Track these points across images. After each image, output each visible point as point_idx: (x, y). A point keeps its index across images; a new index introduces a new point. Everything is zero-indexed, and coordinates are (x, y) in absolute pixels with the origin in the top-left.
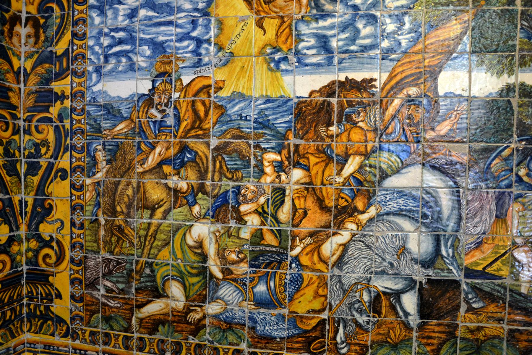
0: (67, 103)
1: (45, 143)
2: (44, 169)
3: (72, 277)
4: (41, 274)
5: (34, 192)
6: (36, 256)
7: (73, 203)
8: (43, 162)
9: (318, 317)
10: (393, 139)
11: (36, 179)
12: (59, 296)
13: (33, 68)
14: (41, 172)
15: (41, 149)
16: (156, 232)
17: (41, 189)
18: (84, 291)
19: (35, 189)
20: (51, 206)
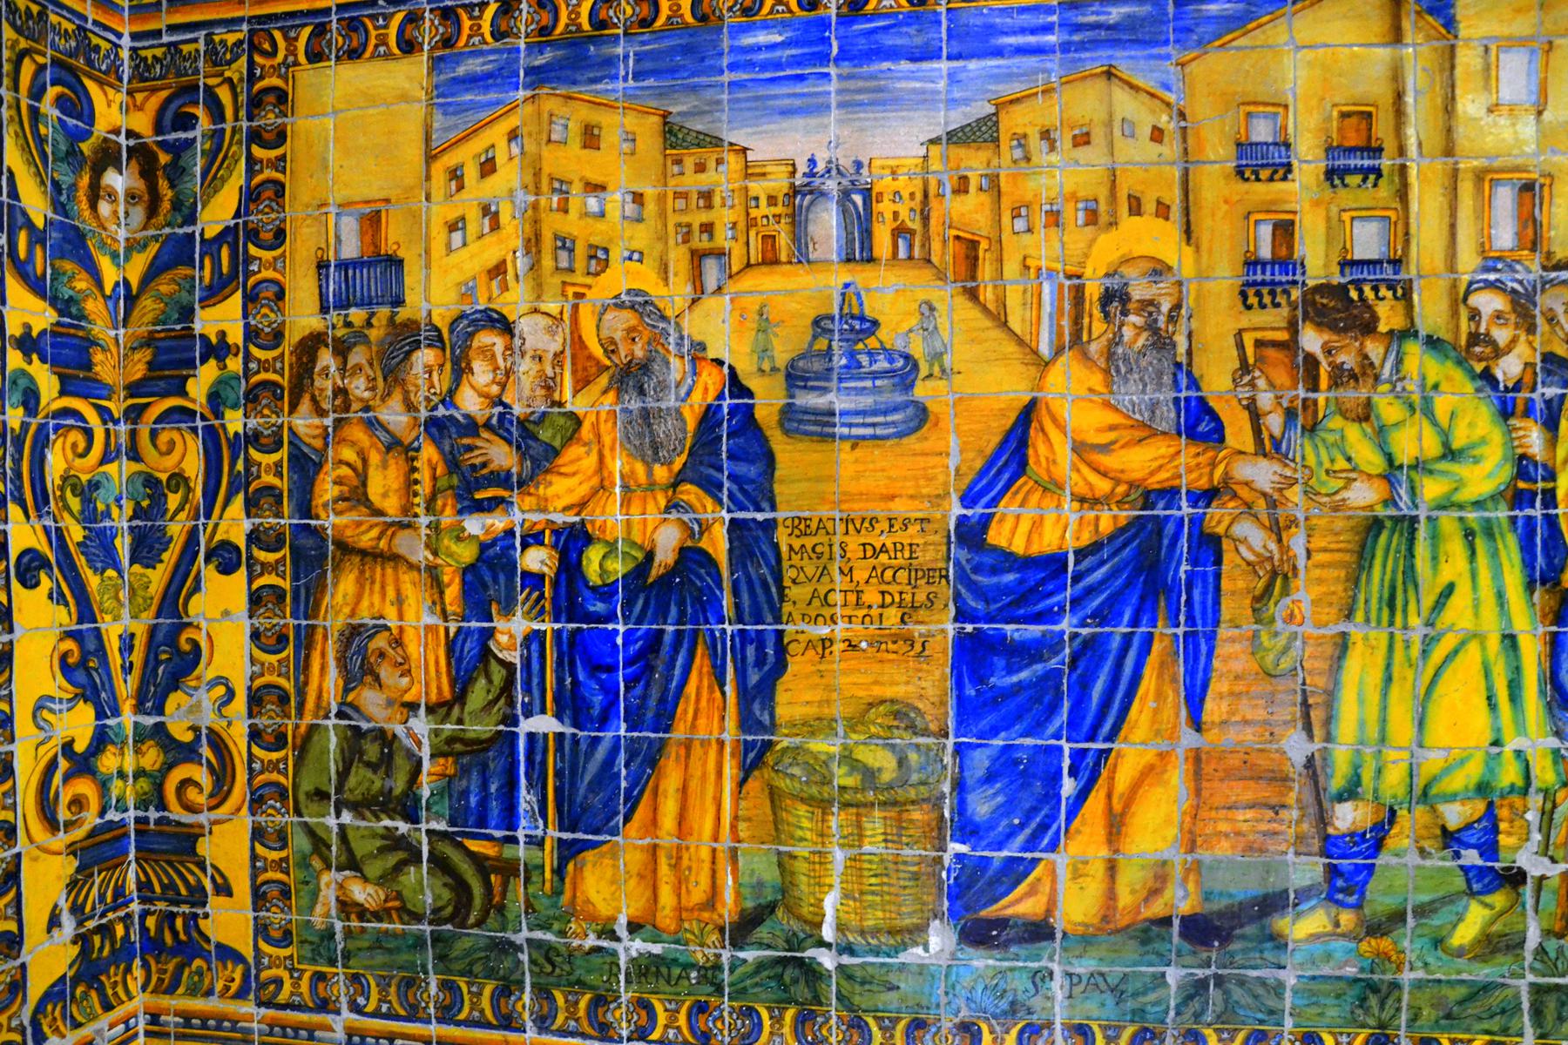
0: (235, 364)
1: (178, 480)
3: (258, 682)
4: (175, 835)
5: (154, 608)
6: (159, 788)
8: (177, 529)
11: (157, 577)
12: (224, 889)
13: (149, 278)
14: (170, 556)
15: (165, 496)
17: (173, 602)
18: (294, 917)
19: (156, 601)
20: (196, 646)
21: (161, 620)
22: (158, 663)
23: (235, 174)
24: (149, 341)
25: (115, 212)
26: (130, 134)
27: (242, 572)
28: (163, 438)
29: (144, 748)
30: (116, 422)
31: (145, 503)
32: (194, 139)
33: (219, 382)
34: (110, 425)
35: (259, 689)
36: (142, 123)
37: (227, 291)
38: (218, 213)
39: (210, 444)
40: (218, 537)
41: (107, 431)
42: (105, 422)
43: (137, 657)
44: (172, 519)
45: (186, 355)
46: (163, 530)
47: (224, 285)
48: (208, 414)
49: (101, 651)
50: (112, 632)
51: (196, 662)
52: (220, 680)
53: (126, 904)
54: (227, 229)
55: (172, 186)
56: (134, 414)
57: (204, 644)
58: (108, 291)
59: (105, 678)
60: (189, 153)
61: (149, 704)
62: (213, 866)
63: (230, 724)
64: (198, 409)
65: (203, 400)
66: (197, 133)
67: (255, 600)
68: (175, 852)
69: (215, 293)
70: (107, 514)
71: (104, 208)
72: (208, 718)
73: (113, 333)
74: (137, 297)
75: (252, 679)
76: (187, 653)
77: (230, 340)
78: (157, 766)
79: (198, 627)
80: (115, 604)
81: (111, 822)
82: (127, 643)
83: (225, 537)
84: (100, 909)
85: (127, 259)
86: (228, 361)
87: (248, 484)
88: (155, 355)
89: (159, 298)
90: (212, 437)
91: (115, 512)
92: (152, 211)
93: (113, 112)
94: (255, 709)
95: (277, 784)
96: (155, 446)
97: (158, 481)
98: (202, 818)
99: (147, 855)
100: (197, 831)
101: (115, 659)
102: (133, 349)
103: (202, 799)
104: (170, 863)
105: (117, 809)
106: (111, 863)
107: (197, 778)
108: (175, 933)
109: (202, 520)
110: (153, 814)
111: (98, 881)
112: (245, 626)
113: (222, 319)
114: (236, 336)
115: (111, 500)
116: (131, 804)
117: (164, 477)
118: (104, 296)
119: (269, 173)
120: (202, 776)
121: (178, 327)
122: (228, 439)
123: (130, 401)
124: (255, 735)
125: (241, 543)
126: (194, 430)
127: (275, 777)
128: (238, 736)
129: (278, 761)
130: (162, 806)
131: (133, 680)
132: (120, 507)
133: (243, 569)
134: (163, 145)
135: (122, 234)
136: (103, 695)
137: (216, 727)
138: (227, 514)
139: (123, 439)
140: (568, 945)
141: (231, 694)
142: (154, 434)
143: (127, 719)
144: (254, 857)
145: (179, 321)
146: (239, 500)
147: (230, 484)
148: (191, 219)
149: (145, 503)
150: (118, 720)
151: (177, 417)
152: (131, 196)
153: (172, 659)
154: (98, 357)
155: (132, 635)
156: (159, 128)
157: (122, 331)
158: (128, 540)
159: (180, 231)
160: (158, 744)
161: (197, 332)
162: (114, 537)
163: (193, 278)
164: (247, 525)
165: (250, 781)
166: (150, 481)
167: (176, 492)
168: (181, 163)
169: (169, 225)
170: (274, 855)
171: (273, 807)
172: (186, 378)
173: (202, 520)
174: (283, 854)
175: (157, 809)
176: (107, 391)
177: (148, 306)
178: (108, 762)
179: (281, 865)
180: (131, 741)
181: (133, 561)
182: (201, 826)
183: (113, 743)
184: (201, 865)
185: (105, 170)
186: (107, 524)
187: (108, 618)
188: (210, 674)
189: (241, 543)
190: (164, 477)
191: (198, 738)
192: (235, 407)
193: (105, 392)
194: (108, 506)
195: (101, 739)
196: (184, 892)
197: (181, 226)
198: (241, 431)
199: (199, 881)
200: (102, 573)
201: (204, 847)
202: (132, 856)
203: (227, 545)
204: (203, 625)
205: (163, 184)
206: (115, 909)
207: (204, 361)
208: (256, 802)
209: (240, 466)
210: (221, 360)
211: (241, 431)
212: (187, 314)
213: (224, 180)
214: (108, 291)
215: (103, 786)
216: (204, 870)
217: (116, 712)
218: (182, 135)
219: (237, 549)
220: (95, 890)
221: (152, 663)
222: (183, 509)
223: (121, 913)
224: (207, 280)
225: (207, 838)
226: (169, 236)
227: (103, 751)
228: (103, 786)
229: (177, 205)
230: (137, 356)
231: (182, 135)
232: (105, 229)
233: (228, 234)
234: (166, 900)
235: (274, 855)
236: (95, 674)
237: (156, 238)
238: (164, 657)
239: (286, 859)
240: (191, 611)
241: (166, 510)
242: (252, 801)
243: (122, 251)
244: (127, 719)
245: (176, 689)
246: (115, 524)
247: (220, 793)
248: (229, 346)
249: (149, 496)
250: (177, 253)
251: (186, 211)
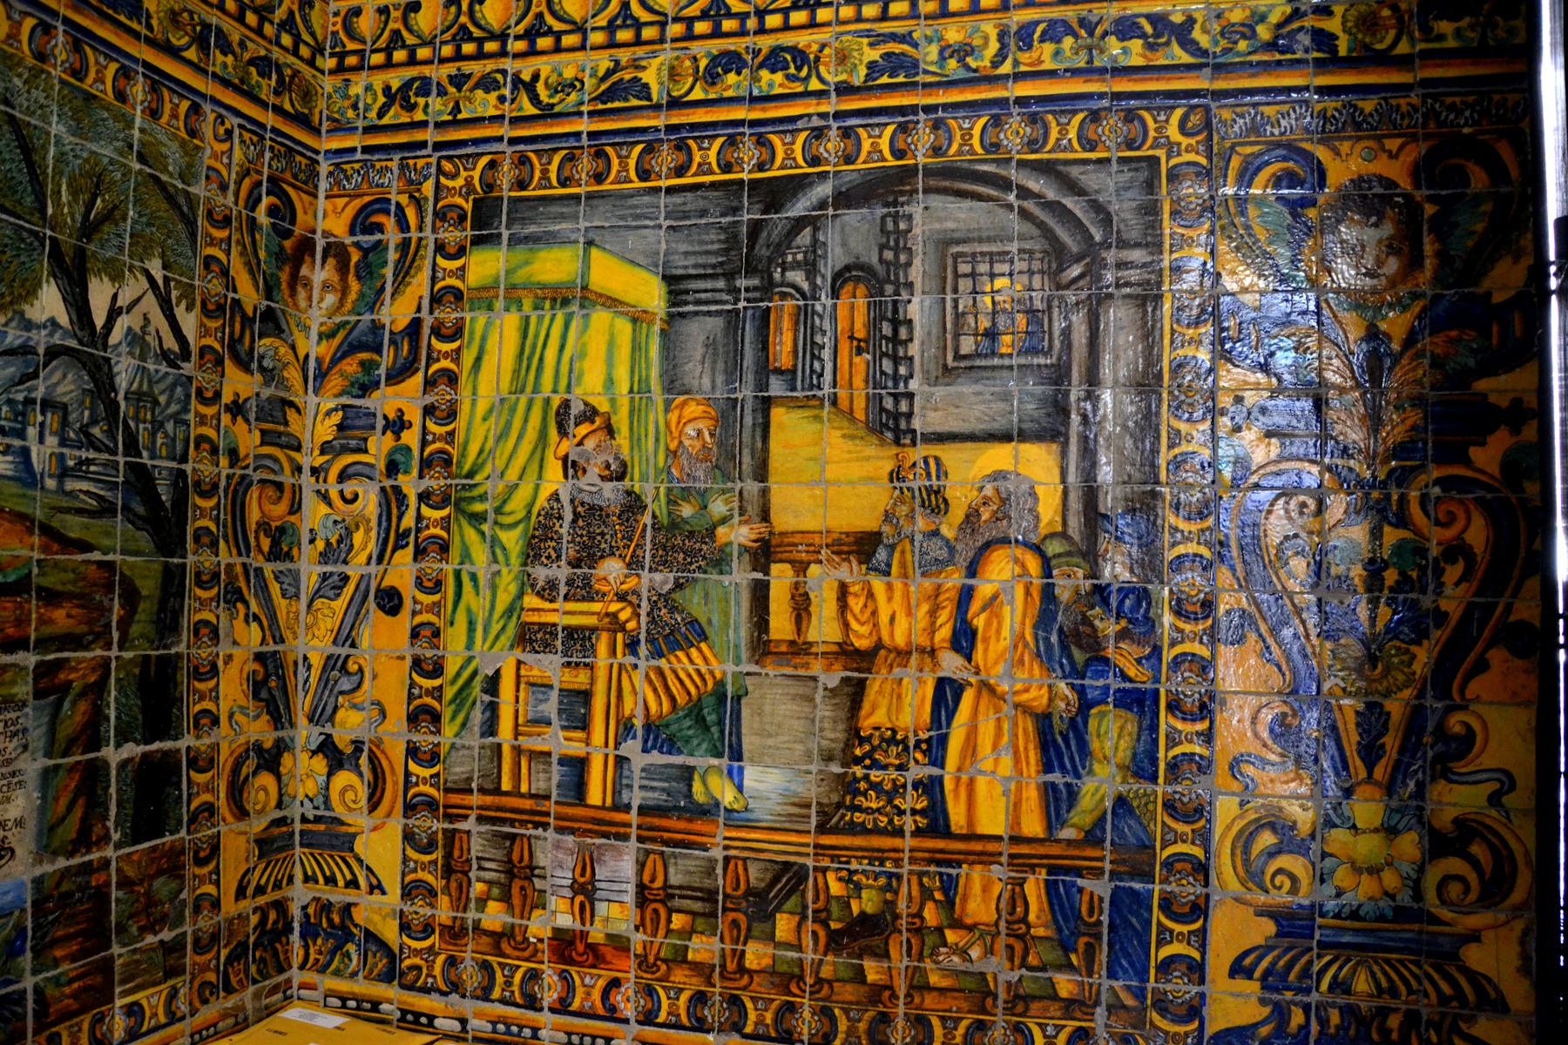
13: (335, 361)
38: (396, 313)
69: (398, 375)
108: (330, 921)
114: (414, 415)
119: (445, 363)
122: (397, 530)
124: (412, 752)
128: (397, 752)
208: (410, 809)
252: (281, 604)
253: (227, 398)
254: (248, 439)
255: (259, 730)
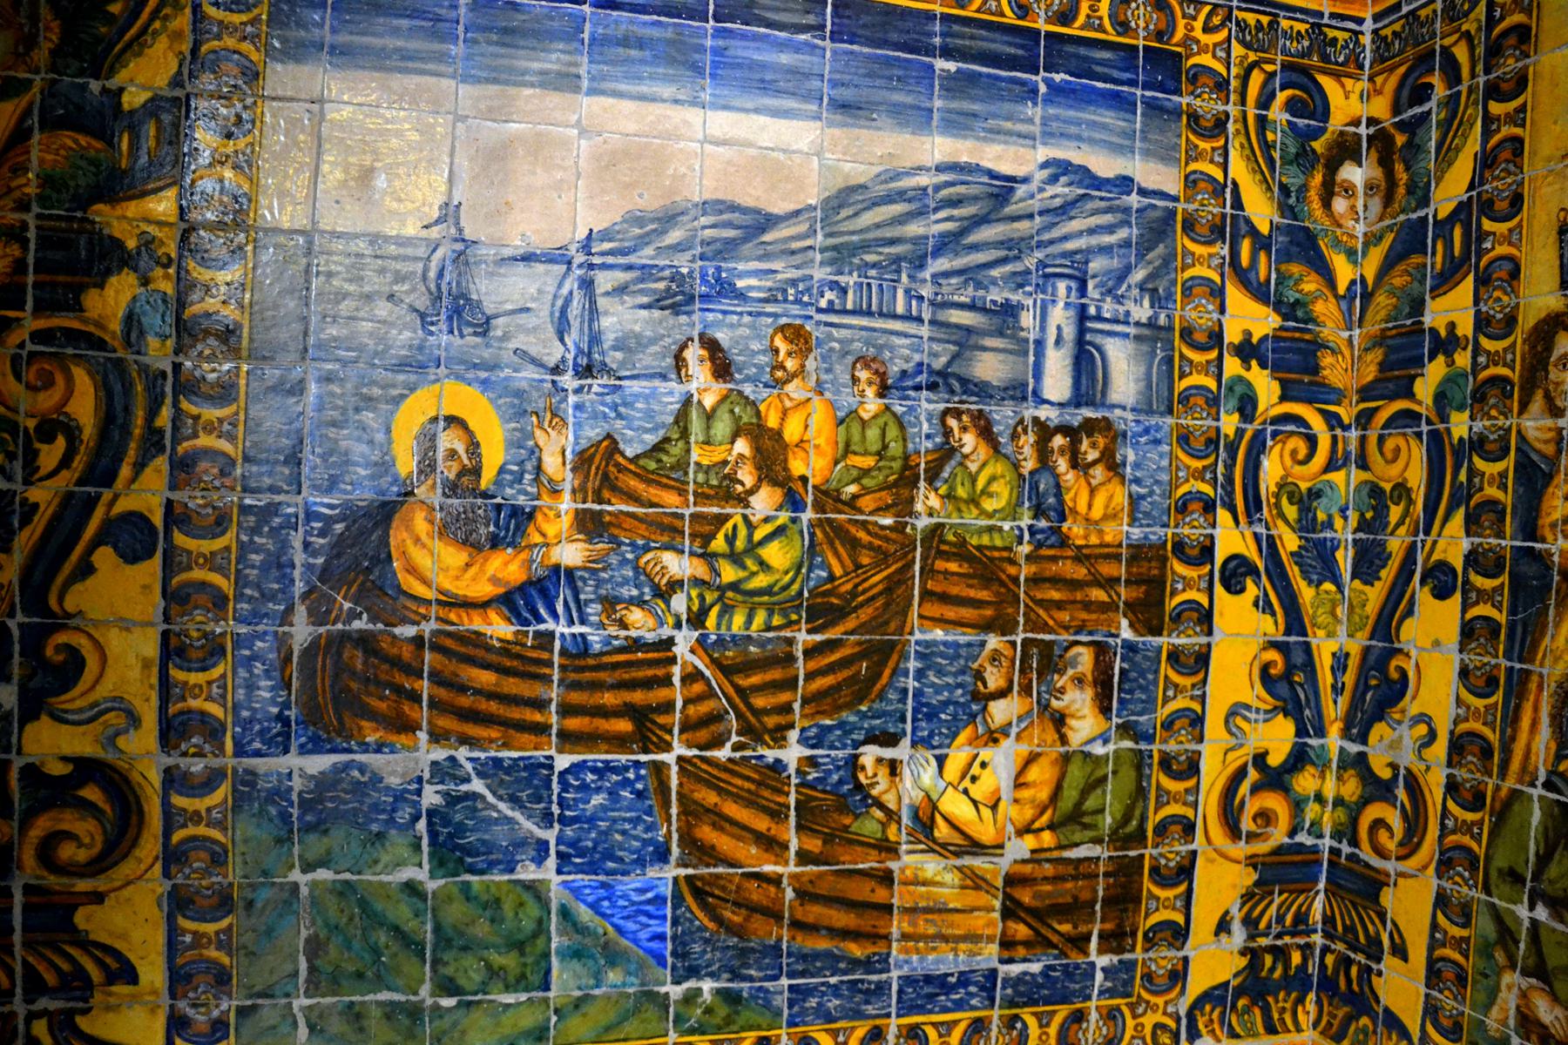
0: (1463, 359)
1: (1402, 491)
2: (1396, 565)
3: (1463, 727)
4: (1362, 877)
5: (1369, 628)
6: (1354, 822)
7: (1201, 675)
8: (1396, 545)
9: (790, 907)
10: (979, 548)
11: (1374, 595)
14: (1388, 574)
15: (1387, 507)
16: (398, 690)
17: (1386, 625)
19: (1371, 622)
20: (1404, 674)
21: (1373, 643)
22: (1367, 688)
23: (1470, 141)
24: (1380, 340)
25: (1353, 207)
26: (1372, 121)
27: (1458, 597)
28: (1390, 444)
29: (1346, 776)
30: (1346, 428)
31: (1369, 515)
32: (1429, 112)
33: (1448, 380)
34: (1338, 432)
35: (1461, 736)
36: (1380, 107)
37: (1458, 276)
38: (1451, 189)
39: (1434, 453)
40: (1435, 557)
41: (1334, 438)
42: (1332, 428)
43: (1349, 678)
44: (1392, 533)
45: (1415, 353)
46: (1383, 544)
47: (1461, 266)
48: (1434, 418)
49: (1309, 666)
50: (1325, 649)
51: (1403, 694)
52: (1423, 718)
53: (1308, 933)
54: (1460, 203)
55: (1407, 169)
56: (1364, 419)
57: (1411, 675)
58: (1341, 290)
59: (1312, 697)
60: (1424, 128)
61: (1355, 731)
62: (1394, 923)
63: (1428, 768)
64: (1424, 412)
65: (1429, 401)
66: (1432, 104)
67: (1468, 632)
68: (1358, 893)
69: (1445, 281)
70: (1329, 524)
71: (1340, 205)
72: (1407, 759)
73: (1346, 334)
74: (1372, 294)
75: (1455, 723)
76: (1395, 682)
77: (1459, 332)
78: (1354, 799)
79: (1408, 655)
80: (1330, 619)
81: (1301, 844)
82: (1340, 662)
83: (1441, 556)
84: (1276, 929)
85: (1364, 254)
86: (1456, 356)
87: (1470, 497)
88: (1386, 355)
89: (1392, 294)
90: (1436, 442)
91: (1338, 523)
92: (1388, 200)
93: (1350, 103)
94: (1456, 758)
95: (1469, 850)
96: (1382, 454)
97: (1382, 491)
98: (1390, 866)
99: (1334, 888)
100: (1382, 878)
101: (1326, 678)
102: (1366, 350)
103: (1391, 846)
104: (1354, 905)
105: (1309, 833)
106: (1292, 887)
107: (1389, 821)
109: (1421, 536)
110: (1346, 849)
111: (1277, 901)
112: (1455, 659)
113: (1453, 309)
115: (1334, 511)
116: (1327, 830)
117: (1387, 487)
118: (1336, 296)
120: (1395, 820)
121: (1409, 322)
122: (1452, 445)
123: (1363, 406)
124: (1452, 787)
125: (1458, 564)
126: (1419, 435)
127: (1467, 840)
128: (1434, 784)
129: (1473, 823)
130: (1354, 843)
131: (1343, 701)
132: (1345, 518)
133: (1458, 596)
134: (1400, 126)
135: (1360, 229)
136: (1307, 712)
137: (1415, 770)
138: (1446, 532)
139: (1353, 447)
140: (1106, 875)
141: (1432, 736)
142: (1381, 440)
143: (1334, 741)
144: (1434, 926)
145: (1409, 316)
146: (1459, 517)
147: (1452, 495)
148: (1425, 202)
149: (1369, 515)
150: (1321, 741)
151: (1400, 422)
152: (1370, 187)
153: (1381, 688)
154: (1327, 360)
155: (1347, 655)
156: (1396, 109)
157: (1357, 331)
158: (1351, 553)
159: (1414, 216)
160: (1358, 775)
161: (1426, 326)
162: (1335, 548)
163: (1425, 266)
164: (1465, 544)
165: (1441, 838)
166: (1375, 491)
167: (1397, 504)
168: (1417, 140)
169: (1403, 211)
170: (1456, 932)
171: (1461, 876)
172: (1412, 379)
173: (1421, 536)
174: (1465, 933)
175: (1350, 844)
176: (1338, 396)
177: (1382, 300)
178: (1305, 782)
179: (1459, 943)
180: (1334, 766)
181: (1353, 577)
182: (1388, 875)
183: (1313, 763)
184: (1382, 915)
185: (1341, 164)
186: (1328, 534)
187: (1321, 633)
188: (1414, 710)
189: (1458, 564)
190: (1387, 487)
191: (1396, 776)
192: (1461, 408)
193: (1332, 397)
194: (1330, 517)
195: (1299, 758)
196: (1340, 928)
197: (1414, 211)
198: (1466, 436)
199: (1378, 933)
200: (1318, 586)
201: (1387, 898)
202: (1321, 886)
203: (1444, 567)
204: (1413, 653)
205: (1399, 168)
206: (1294, 934)
207: (1432, 358)
208: (1445, 865)
209: (1463, 477)
210: (1449, 354)
211: (1466, 436)
212: (1418, 307)
213: (1458, 150)
214: (1341, 290)
215: (1297, 806)
216: (1384, 923)
217: (1321, 732)
218: (1418, 110)
219: (1454, 571)
220: (1274, 908)
221: (1361, 687)
222: (1403, 523)
223: (1301, 941)
224: (1438, 266)
225: (1391, 889)
226: (1402, 224)
227: (1302, 769)
228: (1297, 806)
229: (1410, 190)
230: (1369, 357)
231: (1418, 110)
232: (1340, 226)
233: (1462, 208)
234: (1346, 942)
235: (1456, 932)
236: (1299, 689)
237: (1390, 228)
238: (1373, 682)
239: (1467, 940)
240: (1402, 637)
241: (1388, 523)
242: (1440, 862)
243: (1360, 247)
244: (1334, 741)
245: (1381, 719)
246: (1339, 535)
247: (1410, 845)
248: (1458, 339)
249: (1374, 508)
250: (1410, 241)
251: (1420, 193)
252: (1306, 593)
253: (1232, 335)
254: (1265, 386)
255: (1278, 737)
